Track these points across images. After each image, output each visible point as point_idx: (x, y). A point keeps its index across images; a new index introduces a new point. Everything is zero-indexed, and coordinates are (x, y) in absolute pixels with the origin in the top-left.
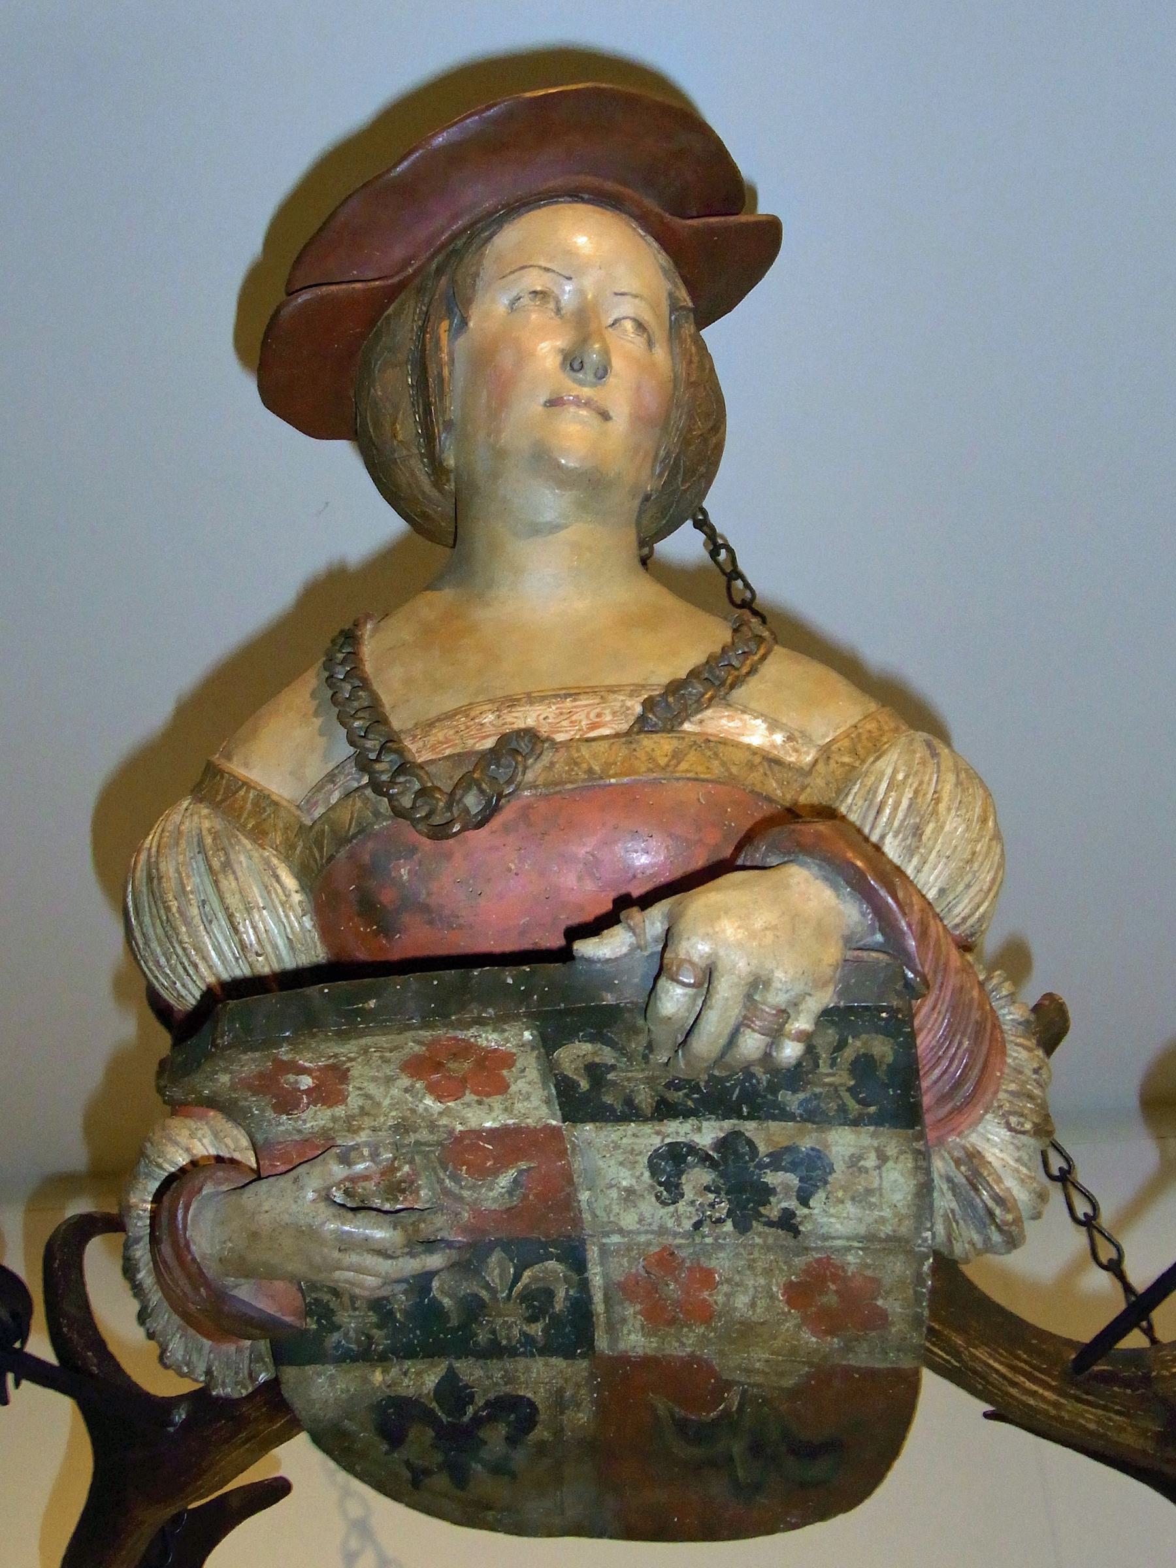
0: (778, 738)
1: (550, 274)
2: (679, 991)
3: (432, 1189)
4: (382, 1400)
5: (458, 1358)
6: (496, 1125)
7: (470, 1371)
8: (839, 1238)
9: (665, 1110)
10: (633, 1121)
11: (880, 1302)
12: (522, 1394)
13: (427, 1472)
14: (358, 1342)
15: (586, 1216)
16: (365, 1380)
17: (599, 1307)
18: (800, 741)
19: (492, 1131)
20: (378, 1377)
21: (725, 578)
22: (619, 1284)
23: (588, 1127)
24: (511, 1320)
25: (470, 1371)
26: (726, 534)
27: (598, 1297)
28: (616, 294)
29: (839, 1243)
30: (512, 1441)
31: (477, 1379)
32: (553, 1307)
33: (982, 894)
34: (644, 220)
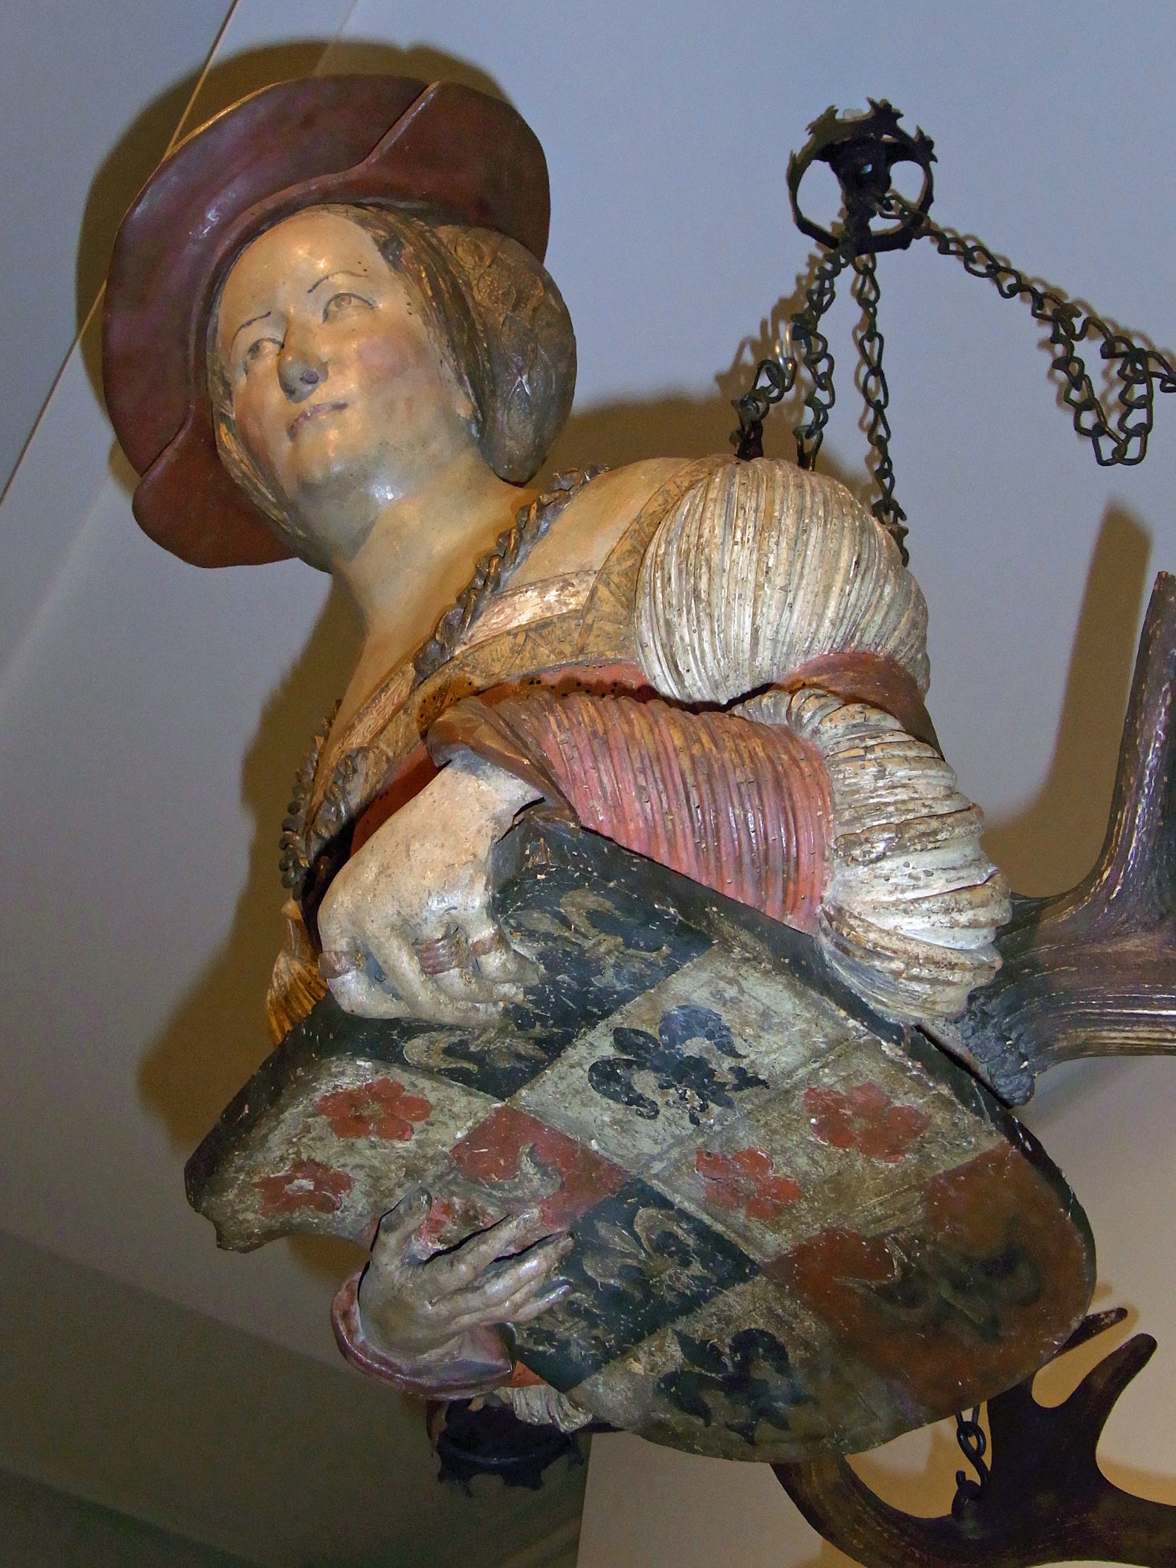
0: (552, 596)
1: (254, 324)
2: (349, 977)
3: (493, 1204)
4: (659, 1385)
5: (673, 1322)
6: (465, 1132)
7: (698, 1326)
8: (797, 1069)
9: (553, 1048)
10: (545, 1069)
11: (898, 1104)
12: (747, 1328)
13: (751, 1428)
14: (593, 1347)
15: (616, 1160)
16: (632, 1375)
17: (719, 1227)
18: (575, 582)
19: (468, 1138)
20: (638, 1368)
21: (987, 280)
22: (706, 1199)
23: (524, 1092)
24: (671, 1271)
25: (698, 1326)
26: (974, 232)
27: (707, 1219)
28: (310, 291)
29: (801, 1072)
30: (783, 1368)
31: (703, 1334)
32: (688, 1246)
33: (821, 595)
34: (325, 199)
